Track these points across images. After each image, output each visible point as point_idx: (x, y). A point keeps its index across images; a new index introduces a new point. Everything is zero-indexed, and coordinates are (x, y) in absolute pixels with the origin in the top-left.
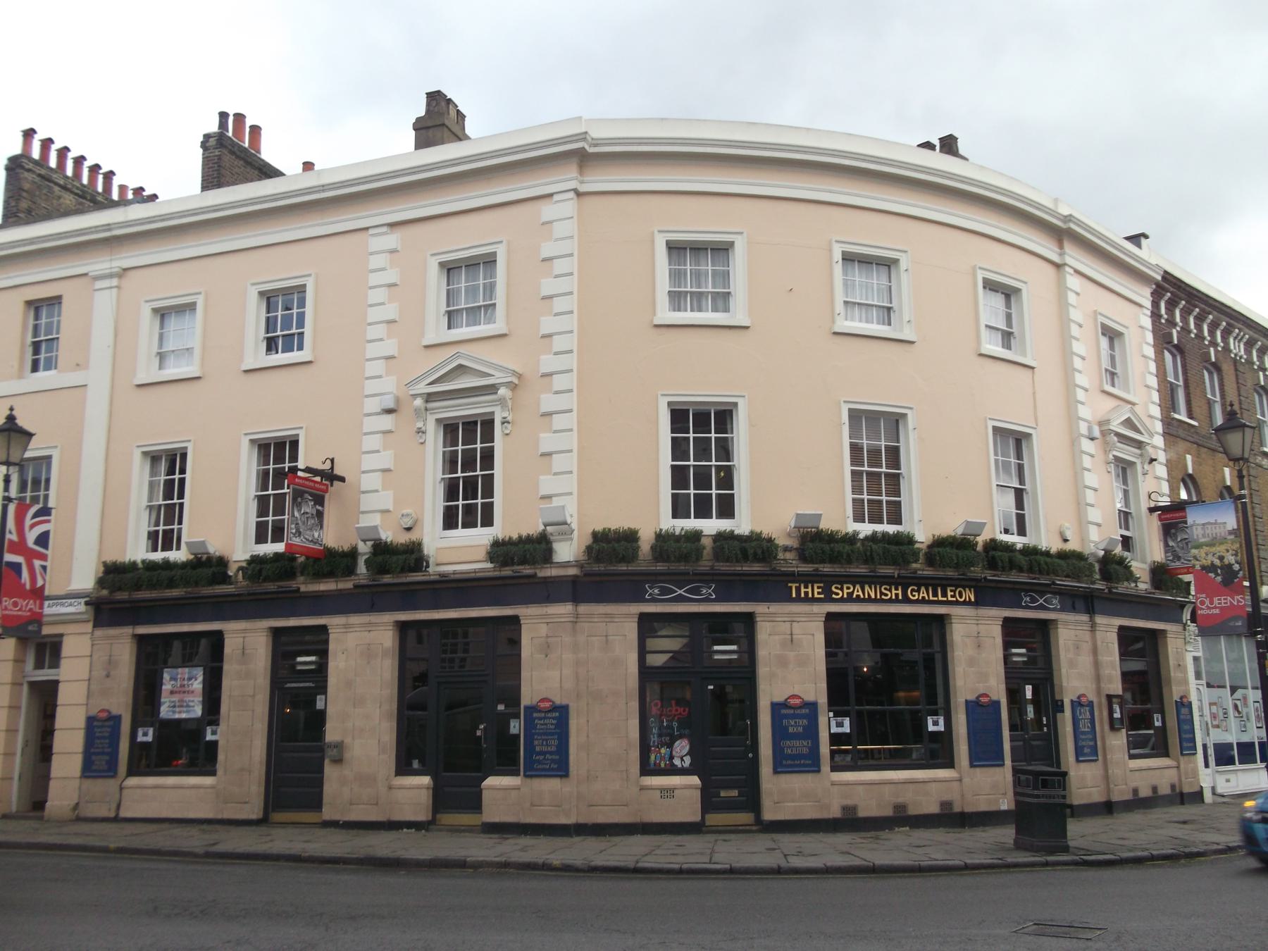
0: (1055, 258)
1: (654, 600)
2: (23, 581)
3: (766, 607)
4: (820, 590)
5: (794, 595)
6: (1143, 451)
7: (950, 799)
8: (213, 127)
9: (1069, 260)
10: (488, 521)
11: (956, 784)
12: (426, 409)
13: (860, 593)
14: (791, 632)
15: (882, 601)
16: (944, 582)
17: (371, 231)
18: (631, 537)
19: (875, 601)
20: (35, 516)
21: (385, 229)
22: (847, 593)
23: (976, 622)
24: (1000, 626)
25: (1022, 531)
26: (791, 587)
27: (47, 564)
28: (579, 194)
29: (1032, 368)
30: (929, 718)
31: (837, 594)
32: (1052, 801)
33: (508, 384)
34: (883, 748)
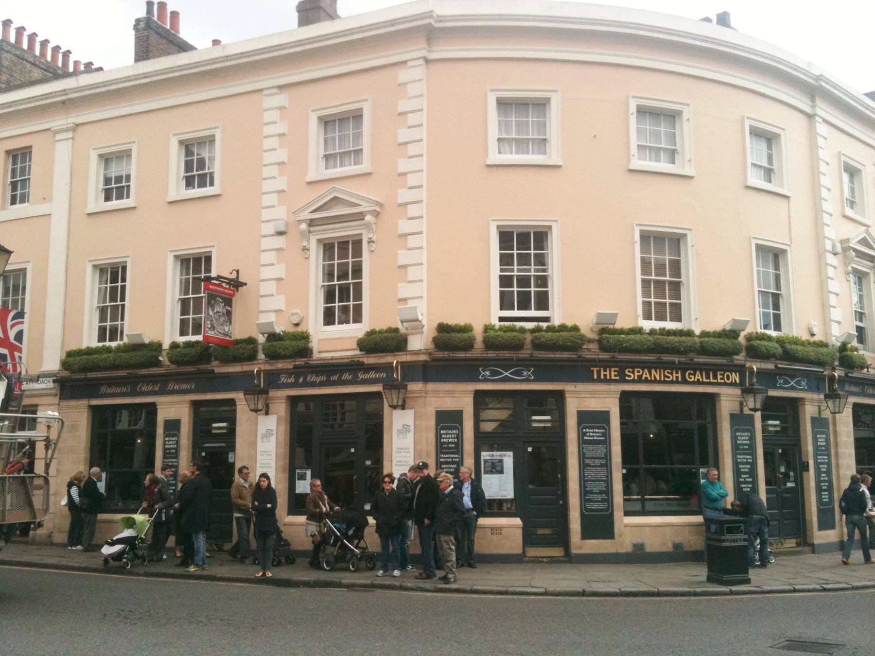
0: (807, 109)
1: (486, 380)
4: (616, 373)
8: (142, 13)
10: (358, 319)
12: (310, 232)
13: (648, 376)
15: (665, 382)
17: (265, 92)
20: (14, 318)
21: (275, 90)
22: (638, 376)
25: (778, 327)
26: (593, 371)
28: (427, 61)
29: (788, 197)
31: (630, 376)
33: (371, 212)
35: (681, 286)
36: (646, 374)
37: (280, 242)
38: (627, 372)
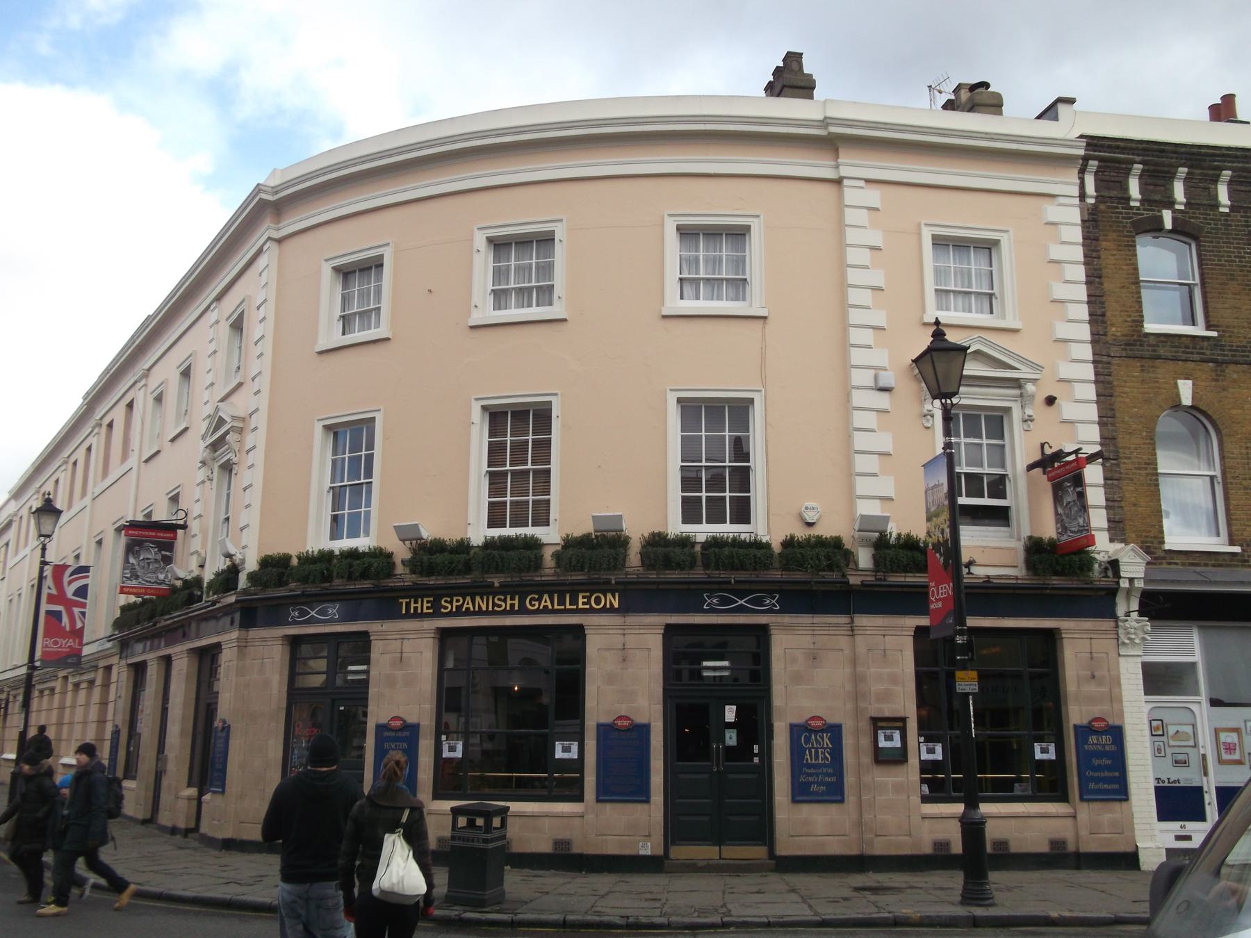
0: (830, 174)
1: (712, 611)
2: (63, 624)
3: (379, 625)
4: (429, 605)
5: (404, 612)
6: (1023, 391)
7: (569, 838)
9: (844, 171)
11: (1069, 822)
13: (471, 606)
14: (402, 650)
15: (494, 613)
16: (576, 588)
17: (1062, 200)
18: (286, 559)
19: (487, 613)
20: (71, 575)
21: (862, 183)
22: (457, 606)
23: (811, 632)
24: (661, 636)
26: (402, 603)
27: (86, 610)
30: (1036, 744)
31: (446, 608)
32: (470, 844)
34: (986, 778)
35: (751, 471)
36: (546, 602)
37: (883, 401)
38: (443, 603)
